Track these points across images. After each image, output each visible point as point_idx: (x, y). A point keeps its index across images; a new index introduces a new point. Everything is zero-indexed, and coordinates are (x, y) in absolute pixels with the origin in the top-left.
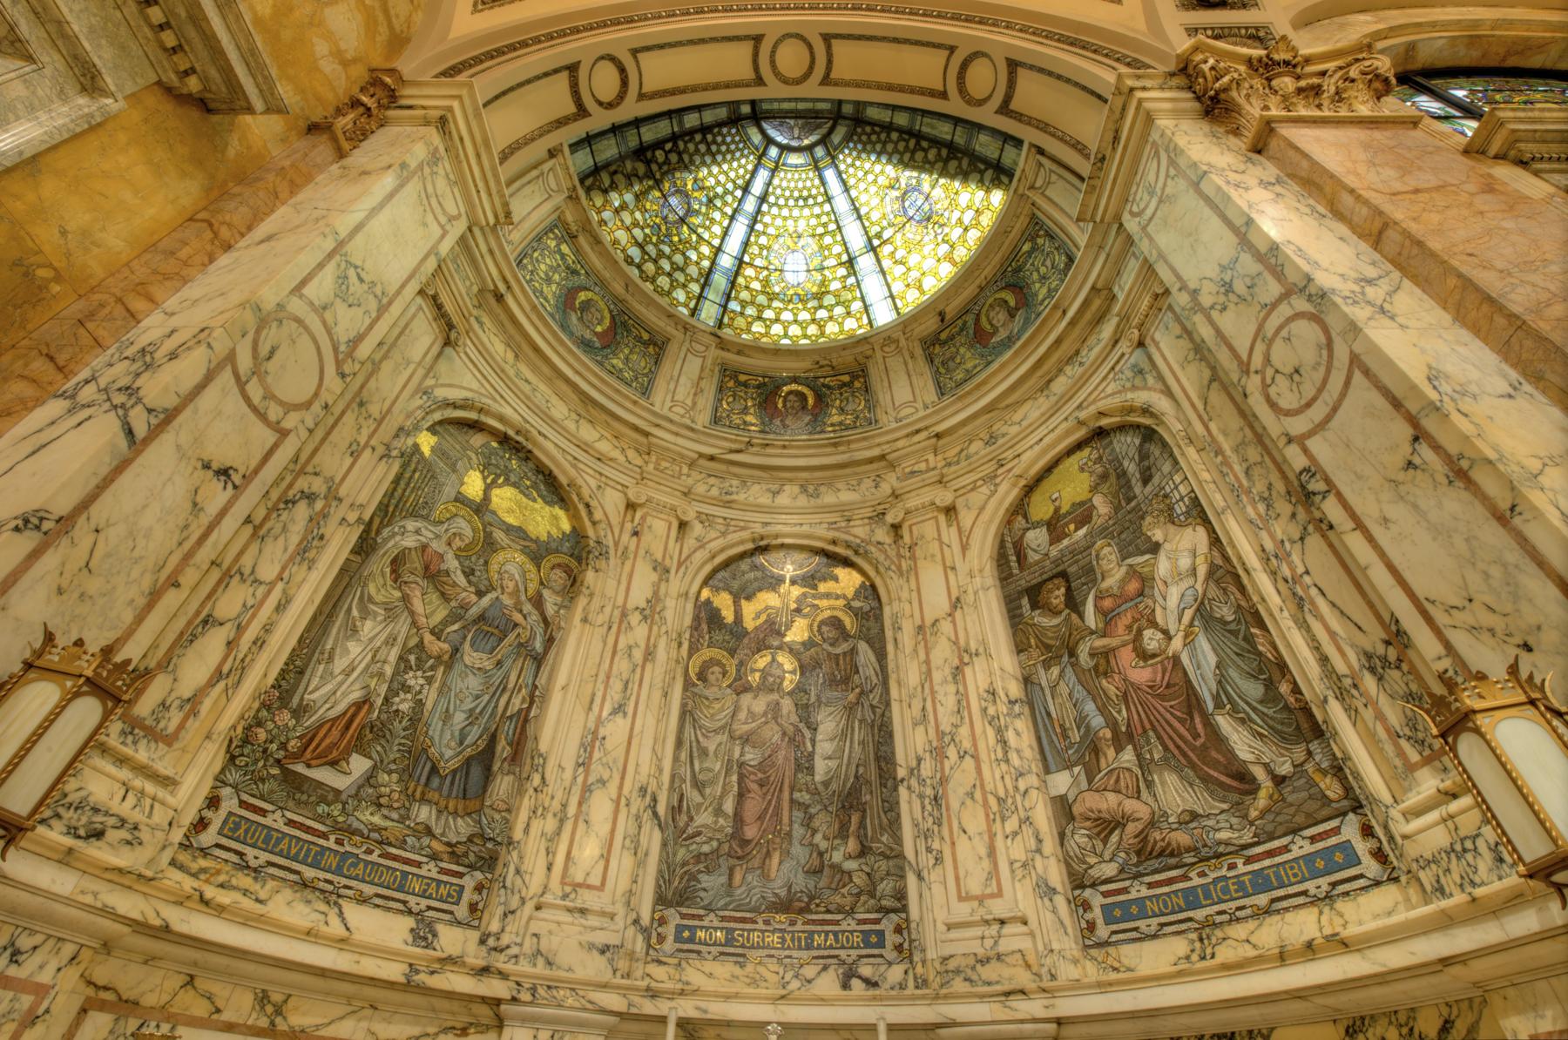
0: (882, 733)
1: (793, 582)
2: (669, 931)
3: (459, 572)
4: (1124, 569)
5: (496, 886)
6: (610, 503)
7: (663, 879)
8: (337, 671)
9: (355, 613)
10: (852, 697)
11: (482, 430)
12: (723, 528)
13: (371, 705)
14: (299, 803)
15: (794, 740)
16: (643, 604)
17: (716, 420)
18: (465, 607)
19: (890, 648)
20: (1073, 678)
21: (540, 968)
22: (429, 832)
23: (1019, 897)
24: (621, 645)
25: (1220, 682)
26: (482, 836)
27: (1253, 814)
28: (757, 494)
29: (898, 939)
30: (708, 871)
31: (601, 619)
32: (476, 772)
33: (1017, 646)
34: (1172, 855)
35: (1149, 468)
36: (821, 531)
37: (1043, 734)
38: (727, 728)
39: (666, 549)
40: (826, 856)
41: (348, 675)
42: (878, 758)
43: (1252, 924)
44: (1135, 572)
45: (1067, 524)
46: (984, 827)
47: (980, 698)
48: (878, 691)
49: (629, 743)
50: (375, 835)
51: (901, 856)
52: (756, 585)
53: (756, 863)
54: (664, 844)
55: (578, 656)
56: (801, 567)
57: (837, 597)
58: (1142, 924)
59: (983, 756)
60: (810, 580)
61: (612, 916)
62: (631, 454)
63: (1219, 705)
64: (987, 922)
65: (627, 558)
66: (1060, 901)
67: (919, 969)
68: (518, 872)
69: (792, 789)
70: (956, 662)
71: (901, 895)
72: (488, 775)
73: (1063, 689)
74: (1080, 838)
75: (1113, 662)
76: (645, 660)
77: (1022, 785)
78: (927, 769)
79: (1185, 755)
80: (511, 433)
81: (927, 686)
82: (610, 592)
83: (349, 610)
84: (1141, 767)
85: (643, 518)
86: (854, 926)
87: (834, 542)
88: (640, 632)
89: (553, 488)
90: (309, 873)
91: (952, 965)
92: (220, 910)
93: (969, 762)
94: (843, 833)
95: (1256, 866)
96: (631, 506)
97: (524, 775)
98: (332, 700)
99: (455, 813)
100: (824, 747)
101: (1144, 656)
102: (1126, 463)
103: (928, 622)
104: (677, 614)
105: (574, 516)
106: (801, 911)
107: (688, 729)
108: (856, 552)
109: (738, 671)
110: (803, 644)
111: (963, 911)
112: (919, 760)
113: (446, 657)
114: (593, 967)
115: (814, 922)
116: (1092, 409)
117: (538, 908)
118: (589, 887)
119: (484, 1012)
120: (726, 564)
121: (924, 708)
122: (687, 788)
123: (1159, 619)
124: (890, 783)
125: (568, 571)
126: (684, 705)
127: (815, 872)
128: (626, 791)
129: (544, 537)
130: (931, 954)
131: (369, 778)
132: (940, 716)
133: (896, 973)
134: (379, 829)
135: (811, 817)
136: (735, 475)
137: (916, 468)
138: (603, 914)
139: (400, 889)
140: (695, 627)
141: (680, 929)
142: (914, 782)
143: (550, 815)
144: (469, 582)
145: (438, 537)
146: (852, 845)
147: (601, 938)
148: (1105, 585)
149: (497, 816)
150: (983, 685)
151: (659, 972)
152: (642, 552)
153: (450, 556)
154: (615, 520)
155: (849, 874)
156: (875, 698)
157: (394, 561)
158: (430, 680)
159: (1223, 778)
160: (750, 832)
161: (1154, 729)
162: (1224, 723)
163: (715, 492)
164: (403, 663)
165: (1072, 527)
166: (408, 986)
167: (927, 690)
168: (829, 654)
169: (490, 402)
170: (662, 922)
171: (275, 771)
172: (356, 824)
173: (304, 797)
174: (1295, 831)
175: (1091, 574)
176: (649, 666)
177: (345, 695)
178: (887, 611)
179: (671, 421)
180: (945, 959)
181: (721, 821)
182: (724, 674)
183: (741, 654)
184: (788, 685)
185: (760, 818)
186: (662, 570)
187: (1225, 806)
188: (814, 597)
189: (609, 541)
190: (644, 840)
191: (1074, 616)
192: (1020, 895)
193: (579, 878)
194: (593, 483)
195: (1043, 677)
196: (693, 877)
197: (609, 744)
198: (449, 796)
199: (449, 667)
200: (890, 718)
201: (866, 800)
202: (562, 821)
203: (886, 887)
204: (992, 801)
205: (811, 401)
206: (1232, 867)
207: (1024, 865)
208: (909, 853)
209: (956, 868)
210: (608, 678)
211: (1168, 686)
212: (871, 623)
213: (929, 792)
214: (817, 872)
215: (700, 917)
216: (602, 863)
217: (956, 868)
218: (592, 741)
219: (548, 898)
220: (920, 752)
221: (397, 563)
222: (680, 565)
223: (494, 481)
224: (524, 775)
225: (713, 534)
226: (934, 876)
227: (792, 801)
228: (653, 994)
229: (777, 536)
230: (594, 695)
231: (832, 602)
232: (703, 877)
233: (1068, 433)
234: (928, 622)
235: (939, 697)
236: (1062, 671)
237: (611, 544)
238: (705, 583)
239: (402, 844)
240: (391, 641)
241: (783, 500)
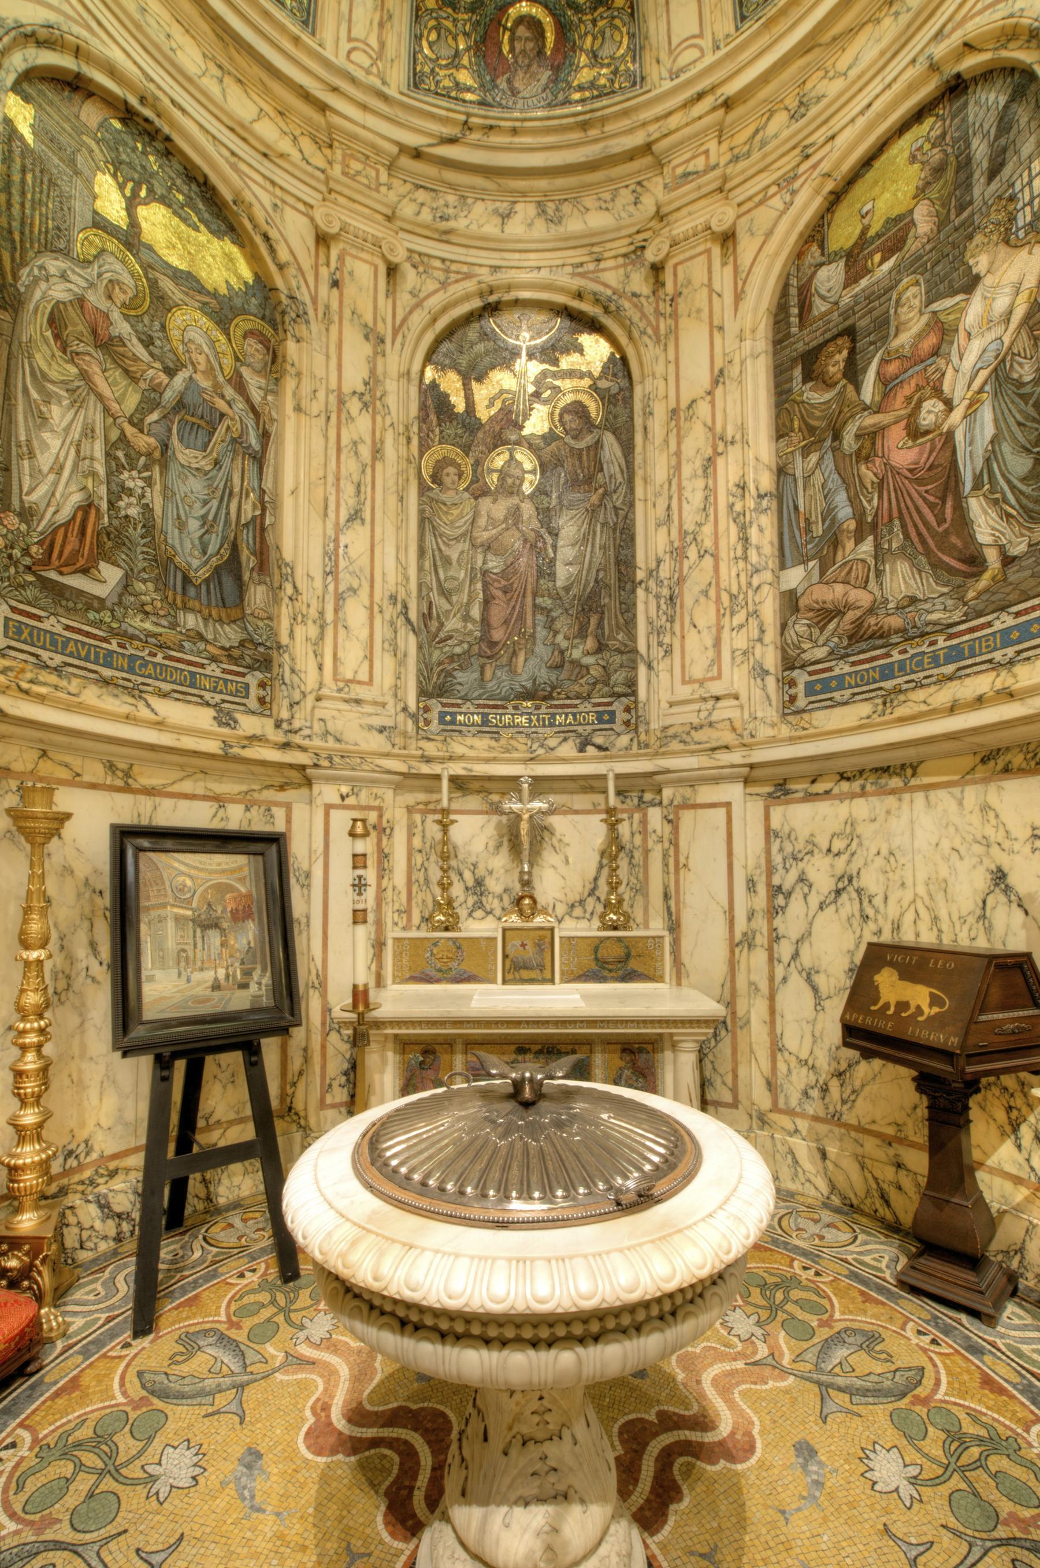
0: (624, 536)
1: (531, 356)
2: (434, 716)
3: (135, 340)
4: (925, 319)
5: (277, 683)
6: (294, 233)
7: (425, 669)
8: (45, 469)
9: (34, 394)
10: (595, 498)
11: (90, 95)
12: (440, 275)
13: (98, 510)
14: (68, 610)
15: (534, 546)
16: (360, 388)
17: (416, 81)
18: (157, 389)
19: (639, 439)
20: (832, 466)
21: (331, 743)
22: (201, 637)
23: (736, 678)
24: (345, 441)
25: (988, 460)
26: (252, 641)
27: (971, 594)
28: (478, 218)
29: (626, 716)
30: (462, 668)
31: (316, 407)
32: (228, 582)
33: (777, 430)
34: (881, 637)
35: (1004, 150)
36: (565, 279)
37: (786, 530)
38: (468, 535)
39: (375, 308)
40: (567, 654)
41: (59, 474)
42: (618, 563)
43: (933, 689)
44: (938, 321)
45: (871, 255)
46: (713, 621)
47: (729, 493)
48: (622, 490)
49: (372, 551)
50: (151, 640)
51: (635, 651)
52: (487, 360)
53: (504, 660)
54: (420, 647)
55: (299, 455)
56: (539, 334)
57: (582, 375)
58: (837, 695)
59: (723, 554)
60: (549, 353)
61: (384, 705)
62: (306, 144)
63: (977, 485)
64: (705, 699)
65: (331, 322)
66: (771, 682)
67: (643, 737)
68: (293, 671)
69: (535, 595)
70: (709, 452)
71: (632, 684)
72: (241, 587)
73: (818, 479)
74: (800, 627)
75: (879, 443)
76: (374, 459)
77: (755, 582)
78: (665, 572)
79: (923, 542)
80: (133, 101)
81: (674, 482)
82: (320, 372)
83: (25, 390)
84: (876, 557)
85: (341, 259)
86: (589, 708)
87: (579, 296)
88: (362, 424)
89: (213, 206)
90: (107, 673)
91: (671, 732)
92: (42, 699)
93: (708, 560)
94: (582, 634)
95: (955, 642)
96: (322, 239)
97: (276, 585)
98: (54, 502)
99: (220, 620)
100: (566, 552)
101: (915, 432)
102: (975, 143)
103: (684, 405)
104: (402, 403)
105: (254, 258)
106: (545, 699)
107: (429, 537)
108: (606, 310)
109: (475, 471)
110: (543, 437)
111: (684, 692)
112: (659, 562)
113: (157, 454)
114: (376, 742)
115: (556, 706)
116: (955, 39)
117: (318, 699)
118: (359, 682)
119: (295, 775)
120: (450, 332)
121: (669, 507)
122: (435, 596)
123: (946, 387)
124: (628, 586)
125: (264, 341)
126: (421, 512)
127: (556, 667)
128: (377, 598)
129: (223, 290)
130: (654, 725)
131: (126, 586)
132: (685, 514)
133: (624, 740)
134: (155, 635)
135: (553, 620)
136: (452, 186)
137: (691, 168)
138: (375, 703)
139: (192, 685)
140: (423, 418)
141: (442, 716)
142: (652, 584)
143: (310, 622)
144: (151, 354)
145: (92, 285)
146: (590, 643)
147: (377, 722)
148: (896, 343)
149: (261, 624)
150: (734, 478)
151: (431, 749)
152: (347, 313)
153: (116, 315)
154: (306, 263)
155: (587, 668)
156: (618, 499)
157: (52, 321)
158: (149, 482)
159: (954, 563)
160: (497, 635)
161: (901, 517)
162: (976, 506)
163: (426, 216)
164: (114, 466)
165: (877, 257)
166: (226, 757)
167: (674, 487)
168: (572, 449)
169: (84, 33)
170: (427, 709)
171: (30, 578)
172: (130, 630)
173: (71, 604)
174: (1002, 609)
175: (883, 327)
176: (379, 466)
177: (66, 497)
178: (638, 392)
179: (353, 80)
180: (665, 728)
181: (470, 626)
182: (460, 475)
183: (476, 451)
184: (527, 489)
185: (506, 622)
186: (375, 338)
187: (945, 590)
188: (555, 375)
189: (304, 296)
190: (401, 642)
191: (850, 388)
192: (736, 678)
193: (349, 675)
194: (266, 199)
195: (799, 467)
196: (449, 674)
197: (353, 552)
198: (209, 604)
199: (164, 467)
200: (633, 520)
201: (607, 603)
202: (322, 627)
203: (619, 677)
204: (725, 598)
205: (550, 37)
206: (933, 643)
207: (745, 653)
208: (642, 647)
209: (683, 657)
210: (338, 480)
211: (930, 469)
212: (620, 409)
213: (665, 592)
214: (559, 667)
215: (458, 706)
216: (366, 664)
217: (683, 657)
218: (332, 556)
219: (325, 691)
220: (661, 554)
221: (56, 321)
222: (395, 332)
223: (135, 193)
224: (276, 585)
225: (431, 286)
226: (662, 666)
227: (535, 605)
228: (428, 760)
229: (509, 288)
230: (326, 500)
231: (576, 383)
232: (458, 674)
233: (912, 88)
234: (684, 405)
235: (687, 494)
236: (821, 458)
237: (308, 300)
238: (428, 359)
239: (181, 648)
240: (89, 432)
241: (516, 228)
